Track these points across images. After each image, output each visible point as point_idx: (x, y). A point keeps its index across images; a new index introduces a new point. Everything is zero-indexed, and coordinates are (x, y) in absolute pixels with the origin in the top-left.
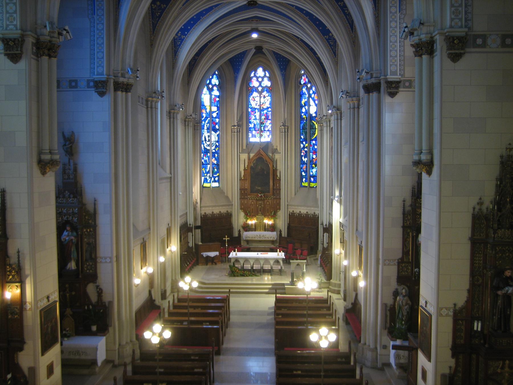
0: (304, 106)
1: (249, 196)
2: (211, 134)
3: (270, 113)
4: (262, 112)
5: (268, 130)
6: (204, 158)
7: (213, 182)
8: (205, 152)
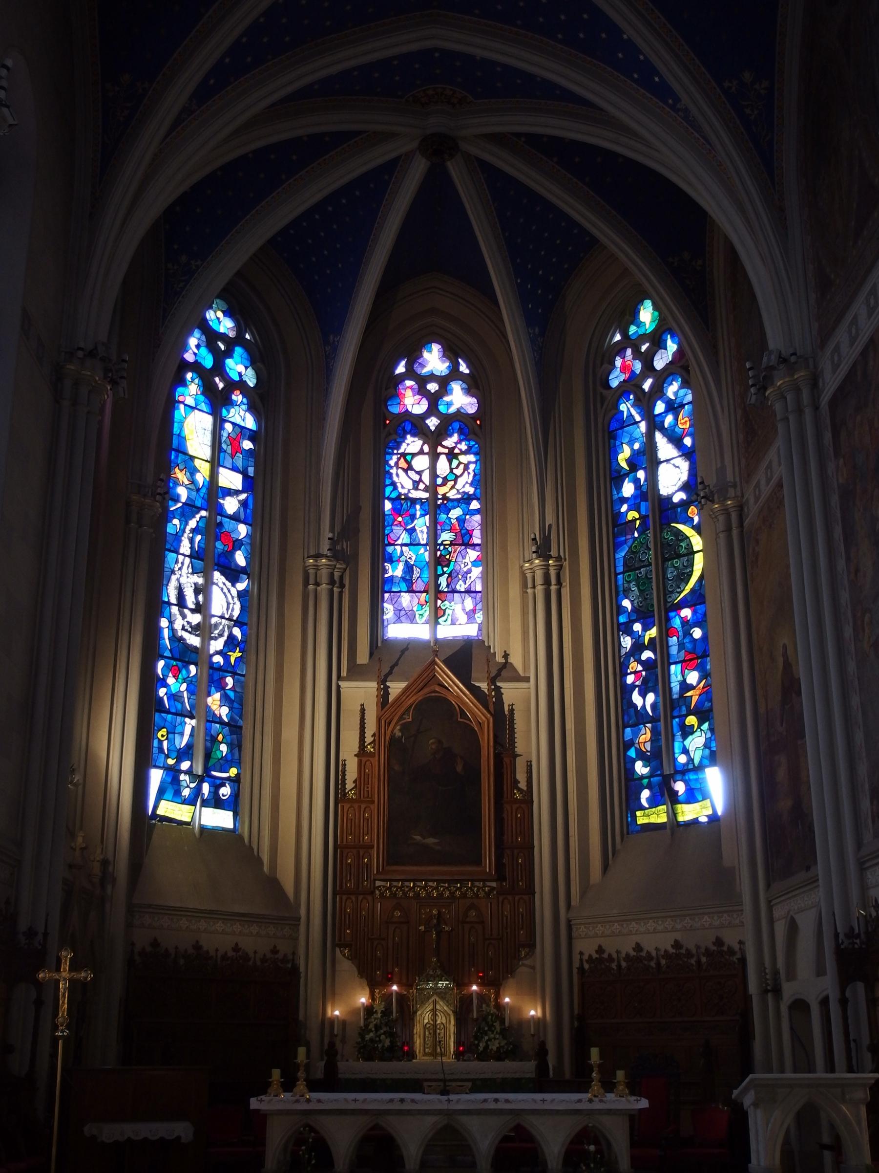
0: (627, 475)
1: (378, 883)
2: (209, 582)
3: (478, 518)
4: (443, 517)
5: (468, 591)
6: (171, 680)
7: (205, 803)
8: (177, 656)
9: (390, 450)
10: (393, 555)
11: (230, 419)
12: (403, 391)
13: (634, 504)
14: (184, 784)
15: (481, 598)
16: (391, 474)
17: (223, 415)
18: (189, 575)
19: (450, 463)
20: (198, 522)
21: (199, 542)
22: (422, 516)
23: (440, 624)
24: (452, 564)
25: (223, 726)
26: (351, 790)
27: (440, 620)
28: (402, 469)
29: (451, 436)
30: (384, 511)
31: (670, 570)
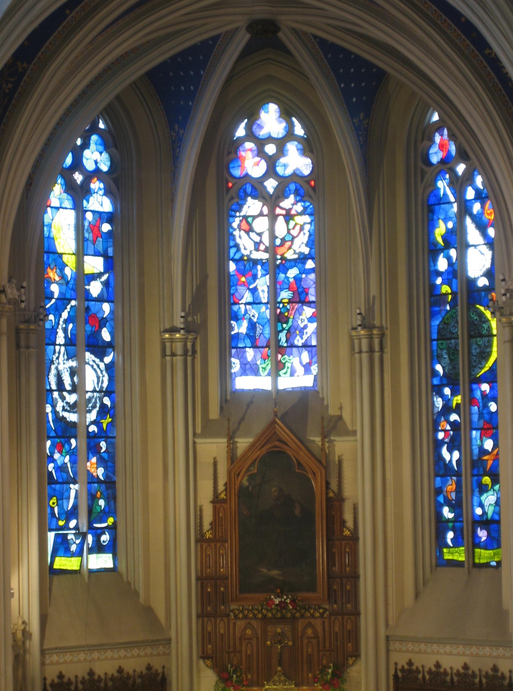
0: (442, 250)
1: (233, 607)
2: (83, 362)
3: (312, 276)
4: (282, 276)
6: (57, 456)
7: (91, 551)
8: (60, 434)
9: (233, 213)
10: (238, 314)
11: (89, 209)
12: (243, 154)
13: (448, 279)
14: (71, 542)
15: (316, 351)
16: (234, 236)
17: (84, 206)
18: (65, 362)
19: (287, 222)
20: (69, 312)
21: (71, 330)
22: (263, 275)
23: (280, 376)
24: (291, 320)
25: (101, 485)
26: (208, 531)
27: (281, 373)
28: (245, 231)
29: (287, 197)
30: (229, 272)
31: (474, 346)
